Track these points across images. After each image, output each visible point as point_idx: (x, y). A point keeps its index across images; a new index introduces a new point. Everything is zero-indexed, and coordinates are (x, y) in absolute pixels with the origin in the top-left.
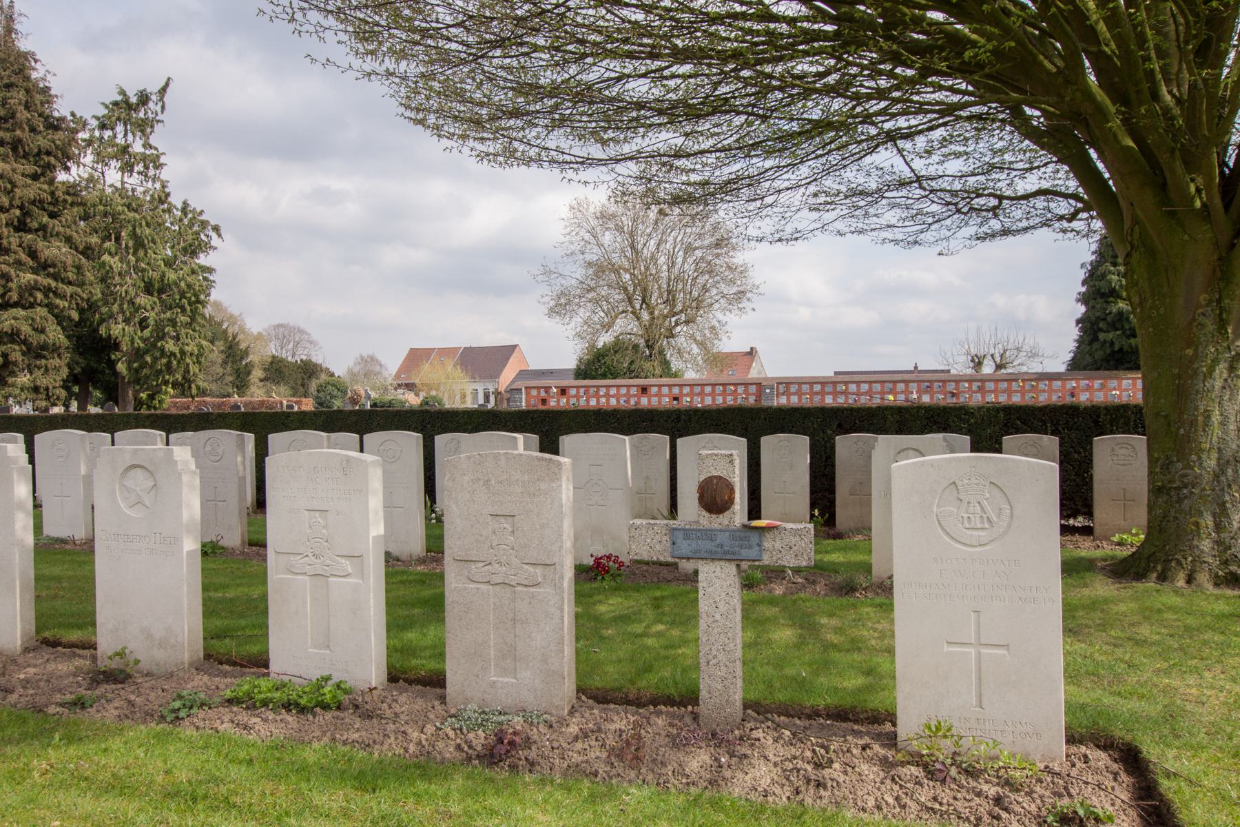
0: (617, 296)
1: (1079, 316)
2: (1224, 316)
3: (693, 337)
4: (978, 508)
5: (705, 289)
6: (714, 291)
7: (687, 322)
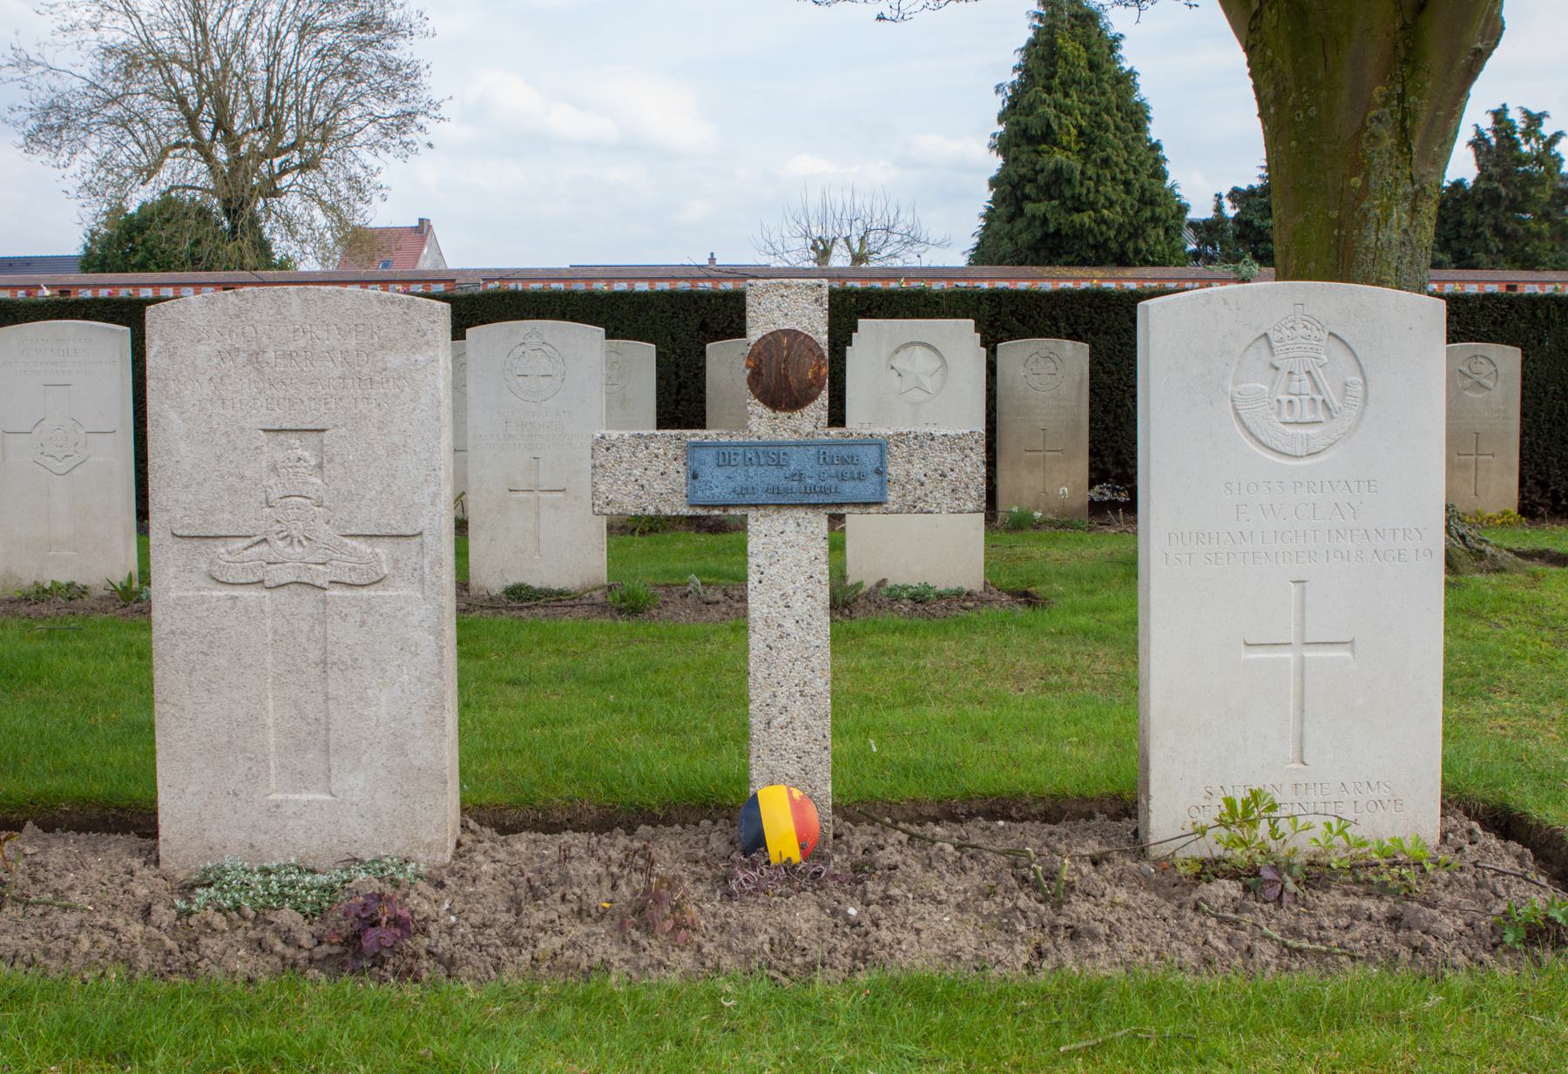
0: (165, 113)
1: (994, 173)
2: (1408, 123)
3: (314, 196)
4: (1307, 382)
5: (337, 106)
6: (355, 111)
7: (303, 167)
